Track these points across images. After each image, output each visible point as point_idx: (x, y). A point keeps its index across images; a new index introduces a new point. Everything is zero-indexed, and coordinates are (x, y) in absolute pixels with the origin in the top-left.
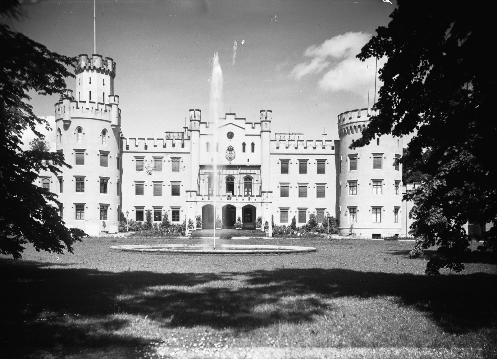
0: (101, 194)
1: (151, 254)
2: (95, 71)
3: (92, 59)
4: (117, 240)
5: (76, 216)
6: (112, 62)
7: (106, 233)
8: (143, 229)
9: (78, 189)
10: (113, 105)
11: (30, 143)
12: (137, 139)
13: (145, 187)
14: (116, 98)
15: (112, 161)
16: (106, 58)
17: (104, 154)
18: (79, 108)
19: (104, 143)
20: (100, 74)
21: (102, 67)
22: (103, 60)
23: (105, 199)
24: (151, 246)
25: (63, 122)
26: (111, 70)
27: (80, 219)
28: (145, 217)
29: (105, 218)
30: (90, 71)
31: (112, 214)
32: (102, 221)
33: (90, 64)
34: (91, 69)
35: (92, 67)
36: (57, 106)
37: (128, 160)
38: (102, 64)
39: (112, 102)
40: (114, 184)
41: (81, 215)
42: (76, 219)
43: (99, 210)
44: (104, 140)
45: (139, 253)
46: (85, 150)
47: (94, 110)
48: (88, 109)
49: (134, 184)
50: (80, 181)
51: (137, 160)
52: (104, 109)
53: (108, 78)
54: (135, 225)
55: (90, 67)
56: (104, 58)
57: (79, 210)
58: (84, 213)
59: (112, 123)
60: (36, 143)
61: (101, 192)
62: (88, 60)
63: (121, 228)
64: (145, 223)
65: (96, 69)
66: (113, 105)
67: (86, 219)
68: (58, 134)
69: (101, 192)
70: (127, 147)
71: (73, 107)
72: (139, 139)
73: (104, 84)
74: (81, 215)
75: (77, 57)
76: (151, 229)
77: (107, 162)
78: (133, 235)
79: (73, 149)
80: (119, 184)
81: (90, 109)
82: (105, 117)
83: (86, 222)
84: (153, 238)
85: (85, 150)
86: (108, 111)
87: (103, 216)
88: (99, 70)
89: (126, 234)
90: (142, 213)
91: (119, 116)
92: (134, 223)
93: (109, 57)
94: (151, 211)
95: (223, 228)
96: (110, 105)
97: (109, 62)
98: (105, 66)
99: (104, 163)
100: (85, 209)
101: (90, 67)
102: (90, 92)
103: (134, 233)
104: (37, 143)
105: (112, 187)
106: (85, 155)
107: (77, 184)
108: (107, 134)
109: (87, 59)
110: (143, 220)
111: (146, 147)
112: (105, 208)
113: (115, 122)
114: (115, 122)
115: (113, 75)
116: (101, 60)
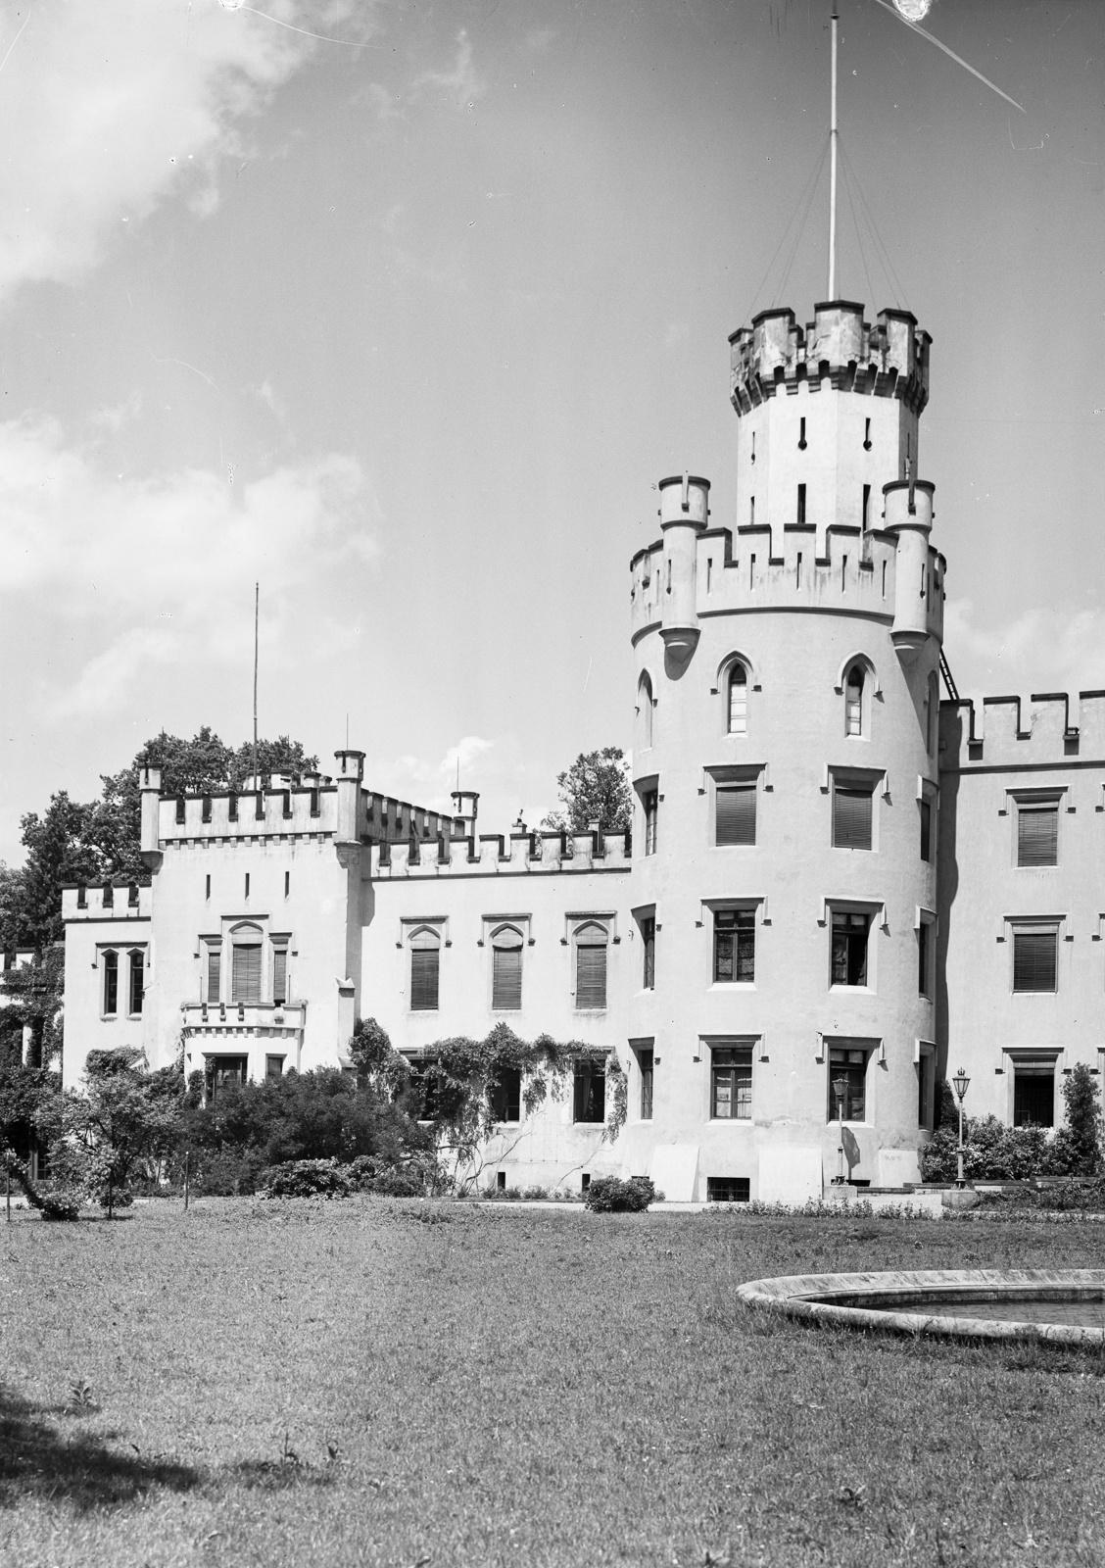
0: (838, 988)
1: (974, 1361)
2: (826, 382)
3: (811, 326)
4: (885, 1226)
5: (715, 1099)
6: (912, 332)
7: (854, 1188)
8: (1047, 1171)
9: (727, 966)
10: (904, 534)
11: (563, 776)
12: (1026, 700)
13: (1063, 947)
14: (920, 496)
15: (894, 821)
16: (879, 315)
17: (854, 785)
18: (735, 565)
19: (854, 727)
20: (852, 397)
21: (862, 359)
22: (866, 327)
23: (854, 1011)
24: (1032, 1276)
25: (662, 640)
26: (903, 372)
27: (734, 1115)
28: (1061, 1105)
29: (855, 1112)
30: (804, 385)
31: (890, 1090)
32: (834, 1124)
33: (802, 351)
34: (809, 378)
35: (813, 367)
36: (641, 564)
37: (983, 814)
38: (862, 346)
39: (900, 515)
40: (903, 934)
41: (735, 1095)
42: (714, 1115)
43: (824, 1068)
44: (855, 711)
45: (895, 1344)
46: (762, 767)
47: (809, 561)
48: (779, 562)
49: (1009, 931)
50: (736, 927)
51: (1021, 811)
52: (854, 563)
53: (887, 410)
54: (1009, 1148)
55: (802, 368)
56: (871, 317)
57: (725, 1072)
58: (749, 1085)
59: (899, 626)
60: (587, 777)
61: (835, 979)
62: (794, 335)
63: (936, 1162)
64: (1062, 1134)
65: (832, 376)
66: (904, 534)
67: (761, 1118)
68: (642, 699)
69: (835, 979)
70: (976, 750)
71: (710, 561)
72: (1035, 698)
73: (867, 445)
74: (735, 1095)
75: (745, 331)
76: (1091, 1167)
77: (869, 823)
78: (990, 1199)
79: (706, 769)
80: (932, 938)
81: (791, 563)
82: (862, 594)
83: (761, 1131)
84: (1084, 1221)
85: (762, 767)
86: (878, 566)
87: (841, 1099)
88: (848, 378)
89: (953, 1193)
90: (1048, 1081)
91: (934, 589)
92: (1005, 1139)
93: (895, 307)
94: (1095, 1072)
95: (709, 1200)
96: (890, 535)
97: (898, 330)
98: (873, 352)
99: (851, 832)
100: (756, 1064)
101: (802, 368)
102: (802, 489)
103: (998, 1189)
104: (591, 777)
105: (889, 952)
106: (760, 794)
107: (721, 939)
108: (871, 684)
109: (791, 331)
110: (1049, 1123)
111: (1072, 743)
112: (856, 1059)
113: (910, 616)
114: (910, 616)
115: (913, 394)
116: (858, 325)
